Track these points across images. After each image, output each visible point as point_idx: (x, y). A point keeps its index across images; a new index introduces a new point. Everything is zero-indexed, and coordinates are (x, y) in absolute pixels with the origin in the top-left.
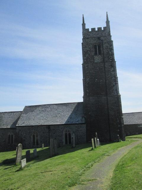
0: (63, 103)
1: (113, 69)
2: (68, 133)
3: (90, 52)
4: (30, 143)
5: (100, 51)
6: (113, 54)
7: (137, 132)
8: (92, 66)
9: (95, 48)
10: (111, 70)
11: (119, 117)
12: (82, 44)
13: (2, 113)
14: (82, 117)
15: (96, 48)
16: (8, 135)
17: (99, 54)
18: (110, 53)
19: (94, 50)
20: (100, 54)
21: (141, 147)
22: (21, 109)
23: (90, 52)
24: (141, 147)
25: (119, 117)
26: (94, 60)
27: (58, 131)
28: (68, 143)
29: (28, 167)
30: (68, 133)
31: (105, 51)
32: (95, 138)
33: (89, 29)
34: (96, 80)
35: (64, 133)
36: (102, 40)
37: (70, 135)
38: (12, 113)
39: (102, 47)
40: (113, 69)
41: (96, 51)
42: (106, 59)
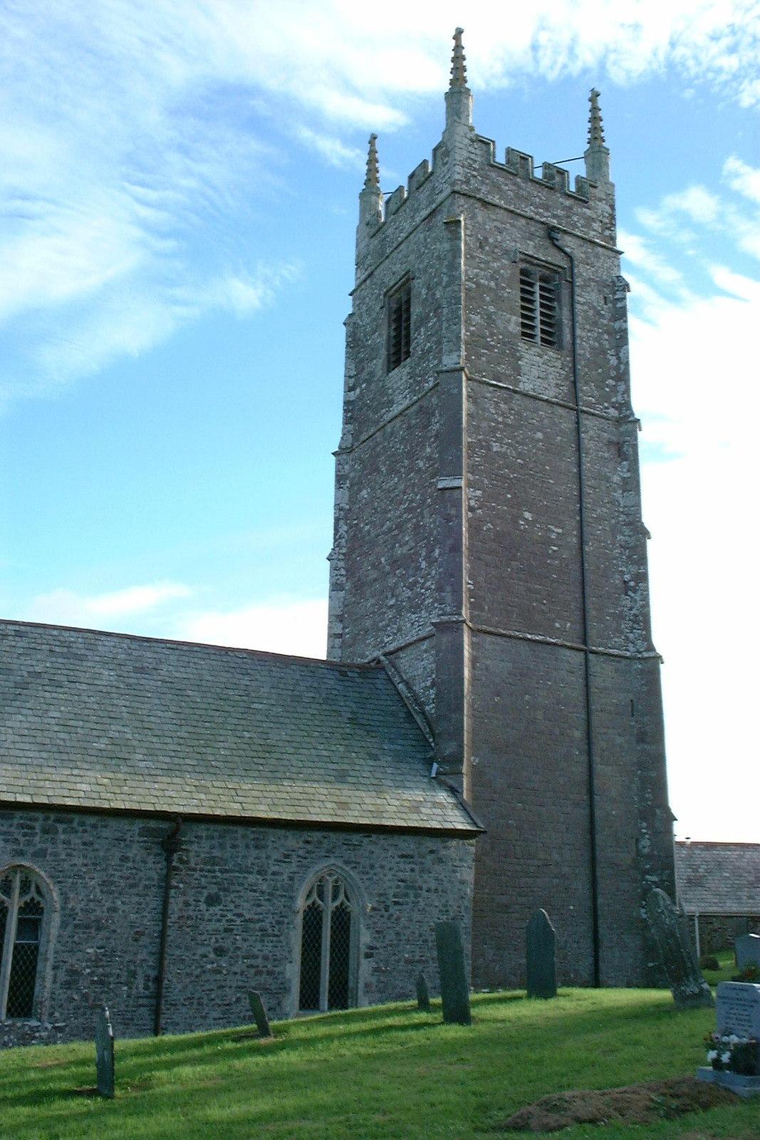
2: (329, 907)
5: (551, 323)
6: (622, 376)
9: (523, 290)
12: (351, 323)
14: (433, 684)
15: (526, 283)
18: (613, 361)
19: (514, 294)
20: (551, 339)
21: (757, 2)
24: (757, 2)
27: (252, 878)
30: (329, 907)
31: (587, 340)
33: (300, 1009)
34: (528, 515)
35: (301, 904)
37: (342, 920)
39: (565, 299)
42: (588, 392)
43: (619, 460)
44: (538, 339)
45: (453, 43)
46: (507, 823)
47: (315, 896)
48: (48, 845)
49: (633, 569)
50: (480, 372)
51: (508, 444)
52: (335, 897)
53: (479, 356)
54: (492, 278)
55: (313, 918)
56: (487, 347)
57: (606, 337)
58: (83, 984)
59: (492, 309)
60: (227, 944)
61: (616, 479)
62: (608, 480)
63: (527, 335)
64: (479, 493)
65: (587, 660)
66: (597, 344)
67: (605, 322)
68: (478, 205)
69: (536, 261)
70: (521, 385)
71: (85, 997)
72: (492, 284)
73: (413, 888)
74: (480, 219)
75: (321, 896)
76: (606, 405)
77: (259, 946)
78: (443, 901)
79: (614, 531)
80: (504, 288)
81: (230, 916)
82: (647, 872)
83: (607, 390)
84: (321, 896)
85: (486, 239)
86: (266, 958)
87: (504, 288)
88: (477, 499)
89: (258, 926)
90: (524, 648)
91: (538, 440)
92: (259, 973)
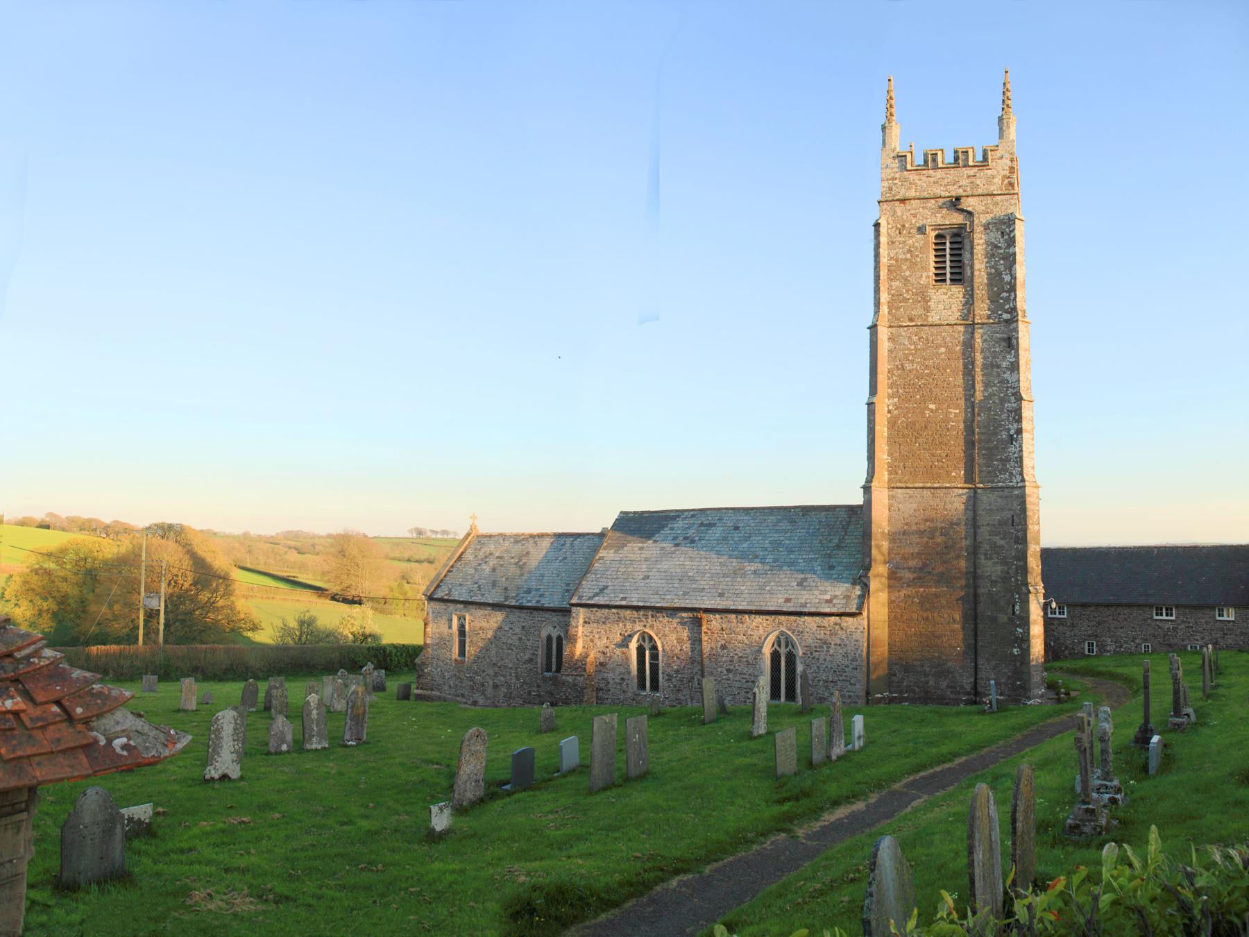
0: (776, 508)
1: (1011, 358)
3: (909, 268)
4: (623, 679)
7: (1146, 640)
8: (915, 338)
10: (1004, 364)
11: (1024, 588)
13: (532, 536)
16: (544, 634)
17: (951, 280)
20: (958, 279)
22: (599, 519)
23: (909, 268)
25: (1024, 588)
26: (927, 309)
28: (783, 698)
29: (581, 772)
30: (783, 651)
32: (836, 929)
34: (932, 406)
35: (767, 650)
36: (970, 214)
37: (791, 658)
38: (569, 540)
40: (1011, 358)
41: (940, 267)
43: (1009, 350)
44: (948, 281)
45: (425, 564)
46: (314, 736)
47: (776, 646)
48: (654, 623)
49: (1015, 425)
50: (899, 319)
51: (918, 362)
52: (787, 646)
53: (898, 308)
54: (909, 251)
55: (775, 656)
56: (906, 300)
57: (1002, 262)
58: (674, 680)
59: (908, 273)
60: (732, 667)
61: (1004, 364)
62: (998, 366)
63: (940, 278)
64: (896, 400)
65: (975, 492)
66: (993, 271)
67: (1002, 251)
68: (897, 204)
69: (944, 227)
70: (930, 319)
71: (675, 686)
72: (908, 256)
73: (825, 643)
74: (899, 214)
75: (779, 645)
76: (1000, 312)
77: (746, 669)
78: (845, 650)
79: (1002, 401)
80: (917, 256)
81: (731, 655)
82: (1018, 626)
83: (1002, 301)
84: (779, 645)
85: (903, 226)
86: (750, 675)
87: (917, 256)
88: (895, 404)
89: (745, 660)
90: (927, 493)
91: (942, 353)
92: (747, 682)
